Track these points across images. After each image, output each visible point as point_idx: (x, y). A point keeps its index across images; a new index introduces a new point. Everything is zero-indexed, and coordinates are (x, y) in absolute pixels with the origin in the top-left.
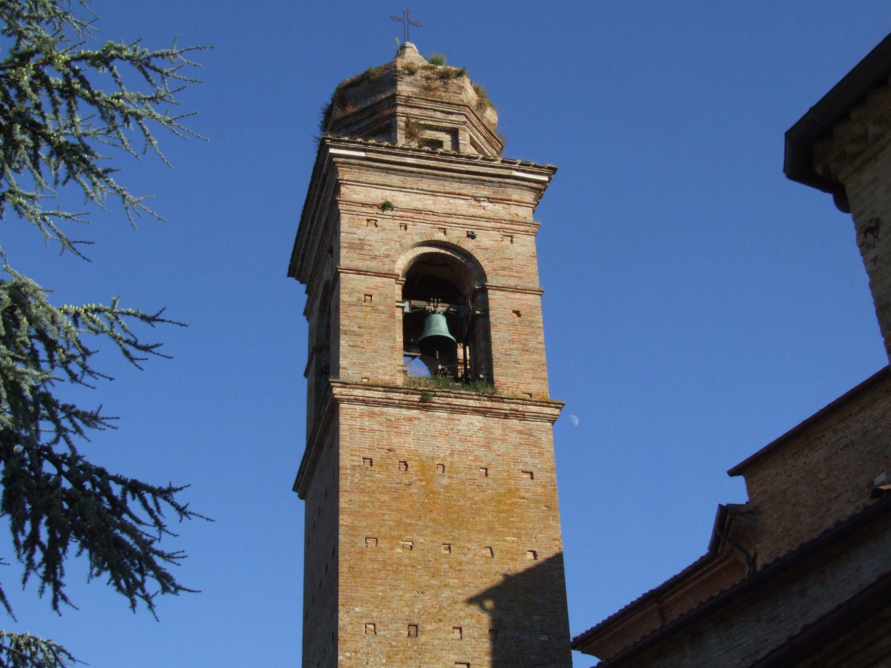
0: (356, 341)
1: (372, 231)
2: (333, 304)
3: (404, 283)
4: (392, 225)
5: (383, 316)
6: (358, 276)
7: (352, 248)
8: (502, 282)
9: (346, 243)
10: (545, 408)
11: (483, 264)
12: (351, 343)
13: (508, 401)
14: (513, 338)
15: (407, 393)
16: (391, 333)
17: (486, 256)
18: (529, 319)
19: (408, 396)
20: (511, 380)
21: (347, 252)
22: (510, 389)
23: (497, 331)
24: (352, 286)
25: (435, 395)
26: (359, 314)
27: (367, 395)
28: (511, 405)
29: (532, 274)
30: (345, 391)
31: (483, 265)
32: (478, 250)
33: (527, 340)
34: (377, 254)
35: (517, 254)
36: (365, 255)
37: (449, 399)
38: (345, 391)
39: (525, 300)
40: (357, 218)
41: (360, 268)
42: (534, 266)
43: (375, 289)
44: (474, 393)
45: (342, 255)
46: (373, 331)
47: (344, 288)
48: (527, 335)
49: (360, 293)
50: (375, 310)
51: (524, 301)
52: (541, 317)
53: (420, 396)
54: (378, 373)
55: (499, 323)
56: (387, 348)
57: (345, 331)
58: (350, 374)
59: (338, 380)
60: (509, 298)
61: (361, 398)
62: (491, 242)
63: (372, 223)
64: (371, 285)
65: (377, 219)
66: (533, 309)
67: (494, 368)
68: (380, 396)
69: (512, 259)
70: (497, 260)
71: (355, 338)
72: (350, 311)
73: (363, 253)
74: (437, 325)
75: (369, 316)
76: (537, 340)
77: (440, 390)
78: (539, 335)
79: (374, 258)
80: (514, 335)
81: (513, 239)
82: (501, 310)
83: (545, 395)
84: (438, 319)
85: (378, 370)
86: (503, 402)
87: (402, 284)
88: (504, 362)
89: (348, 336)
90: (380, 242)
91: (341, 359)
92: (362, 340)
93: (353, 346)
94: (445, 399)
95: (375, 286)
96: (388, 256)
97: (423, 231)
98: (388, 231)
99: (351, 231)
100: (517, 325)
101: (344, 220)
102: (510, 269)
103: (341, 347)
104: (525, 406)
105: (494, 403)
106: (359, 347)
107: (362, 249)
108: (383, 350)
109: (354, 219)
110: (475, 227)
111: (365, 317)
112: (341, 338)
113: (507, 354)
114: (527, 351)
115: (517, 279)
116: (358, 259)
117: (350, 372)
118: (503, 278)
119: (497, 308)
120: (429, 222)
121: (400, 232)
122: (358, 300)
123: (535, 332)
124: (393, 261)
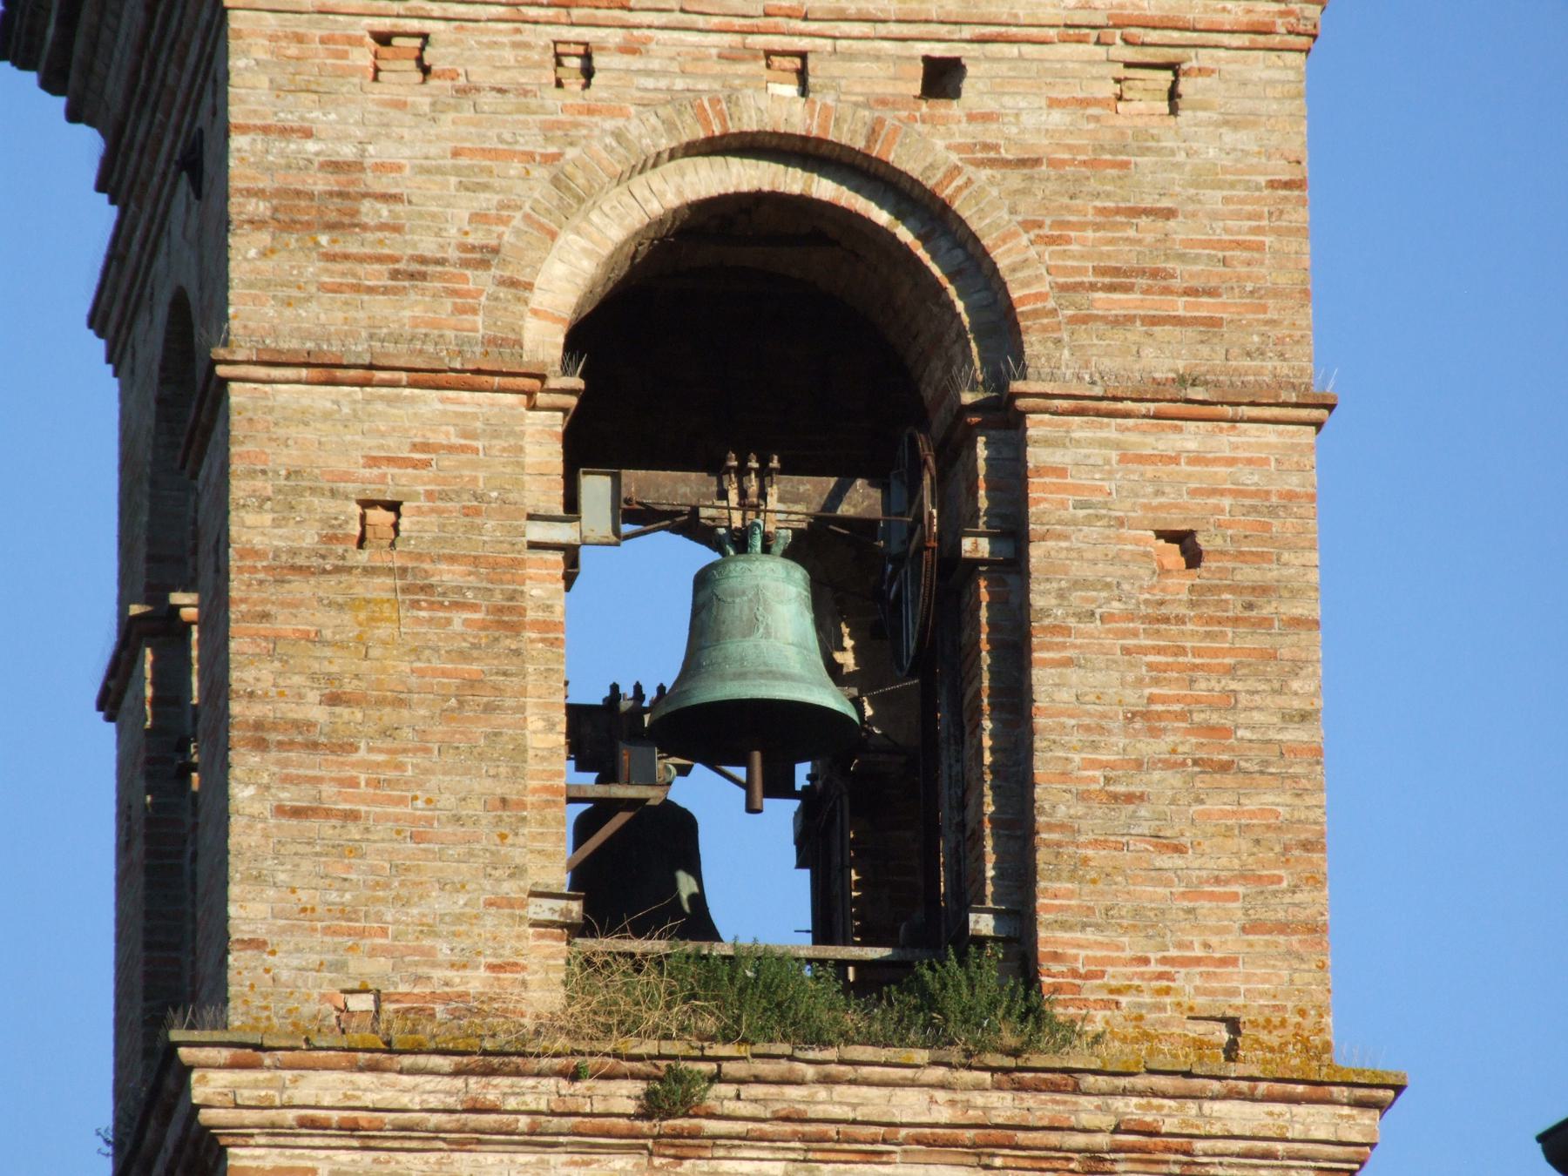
0: (316, 780)
1: (400, 105)
2: (139, 847)
3: (572, 401)
4: (509, 55)
5: (458, 618)
6: (323, 397)
7: (290, 226)
8: (1107, 364)
9: (259, 194)
10: (1301, 1110)
11: (1003, 259)
12: (288, 796)
13: (1102, 1082)
14: (1151, 699)
15: (575, 1076)
16: (498, 719)
17: (1027, 208)
18: (1248, 574)
19: (580, 1086)
20: (1131, 945)
21: (265, 254)
22: (1124, 1000)
23: (1068, 663)
24: (285, 458)
25: (717, 1078)
26: (328, 622)
27: (368, 1099)
28: (1119, 1103)
29: (1276, 293)
30: (250, 1084)
31: (1003, 264)
32: (985, 173)
33: (1229, 701)
34: (427, 245)
35: (1204, 178)
36: (361, 259)
37: (792, 1092)
38: (256, 1085)
39: (1231, 462)
40: (317, 33)
41: (332, 350)
42: (1292, 245)
43: (415, 465)
44: (922, 1056)
45: (238, 269)
46: (405, 713)
47: (251, 474)
48: (1231, 671)
49: (333, 493)
50: (417, 590)
51: (1222, 470)
52: (1314, 557)
53: (639, 1087)
54: (429, 953)
55: (1079, 616)
56: (474, 808)
57: (259, 725)
58: (285, 975)
59: (217, 1036)
60: (1141, 459)
61: (335, 1116)
62: (1057, 118)
63: (400, 55)
64: (391, 442)
65: (427, 26)
66: (1272, 511)
67: (1042, 884)
68: (433, 1102)
69: (1169, 214)
70: (1082, 226)
71: (304, 763)
72: (283, 604)
73: (353, 249)
74: (752, 625)
75: (383, 631)
76: (1282, 701)
77: (744, 1050)
78: (1297, 667)
79: (413, 273)
80: (1156, 682)
81: (1185, 86)
82: (1094, 532)
83: (1308, 1023)
84: (758, 591)
85: (427, 942)
86: (1077, 1090)
87: (564, 410)
88: (1096, 843)
89: (274, 755)
90: (440, 171)
91: (234, 891)
92: (349, 772)
93: (297, 813)
94: (773, 1089)
95: (415, 447)
96: (481, 258)
97: (680, 84)
98: (488, 100)
99: (291, 119)
100: (1180, 620)
101: (245, 53)
102: (1154, 274)
103: (236, 825)
104: (1192, 1107)
105: (1029, 1099)
106: (328, 813)
107: (343, 225)
108: (457, 819)
109: (300, 39)
110: (967, 32)
111: (359, 639)
112: (237, 772)
113: (1115, 797)
114: (1225, 767)
115: (1191, 333)
116: (323, 287)
117: (284, 964)
118: (1117, 337)
119: (1074, 522)
120: (715, 21)
121: (553, 98)
122: (331, 539)
123: (1271, 656)
124: (513, 283)
